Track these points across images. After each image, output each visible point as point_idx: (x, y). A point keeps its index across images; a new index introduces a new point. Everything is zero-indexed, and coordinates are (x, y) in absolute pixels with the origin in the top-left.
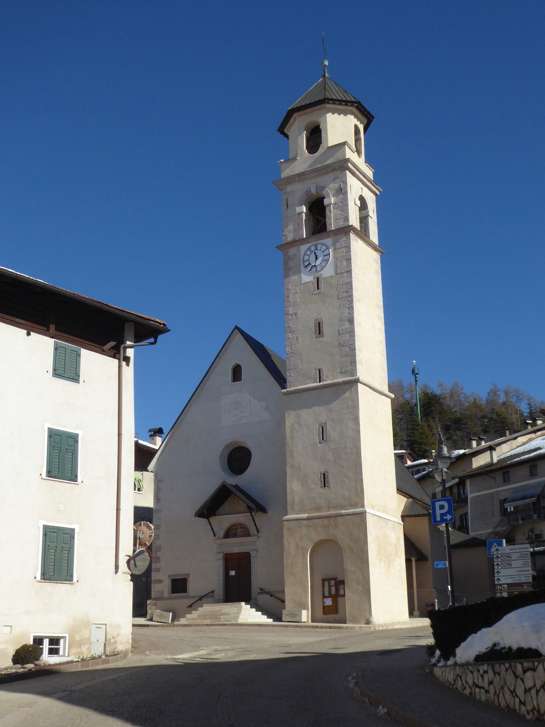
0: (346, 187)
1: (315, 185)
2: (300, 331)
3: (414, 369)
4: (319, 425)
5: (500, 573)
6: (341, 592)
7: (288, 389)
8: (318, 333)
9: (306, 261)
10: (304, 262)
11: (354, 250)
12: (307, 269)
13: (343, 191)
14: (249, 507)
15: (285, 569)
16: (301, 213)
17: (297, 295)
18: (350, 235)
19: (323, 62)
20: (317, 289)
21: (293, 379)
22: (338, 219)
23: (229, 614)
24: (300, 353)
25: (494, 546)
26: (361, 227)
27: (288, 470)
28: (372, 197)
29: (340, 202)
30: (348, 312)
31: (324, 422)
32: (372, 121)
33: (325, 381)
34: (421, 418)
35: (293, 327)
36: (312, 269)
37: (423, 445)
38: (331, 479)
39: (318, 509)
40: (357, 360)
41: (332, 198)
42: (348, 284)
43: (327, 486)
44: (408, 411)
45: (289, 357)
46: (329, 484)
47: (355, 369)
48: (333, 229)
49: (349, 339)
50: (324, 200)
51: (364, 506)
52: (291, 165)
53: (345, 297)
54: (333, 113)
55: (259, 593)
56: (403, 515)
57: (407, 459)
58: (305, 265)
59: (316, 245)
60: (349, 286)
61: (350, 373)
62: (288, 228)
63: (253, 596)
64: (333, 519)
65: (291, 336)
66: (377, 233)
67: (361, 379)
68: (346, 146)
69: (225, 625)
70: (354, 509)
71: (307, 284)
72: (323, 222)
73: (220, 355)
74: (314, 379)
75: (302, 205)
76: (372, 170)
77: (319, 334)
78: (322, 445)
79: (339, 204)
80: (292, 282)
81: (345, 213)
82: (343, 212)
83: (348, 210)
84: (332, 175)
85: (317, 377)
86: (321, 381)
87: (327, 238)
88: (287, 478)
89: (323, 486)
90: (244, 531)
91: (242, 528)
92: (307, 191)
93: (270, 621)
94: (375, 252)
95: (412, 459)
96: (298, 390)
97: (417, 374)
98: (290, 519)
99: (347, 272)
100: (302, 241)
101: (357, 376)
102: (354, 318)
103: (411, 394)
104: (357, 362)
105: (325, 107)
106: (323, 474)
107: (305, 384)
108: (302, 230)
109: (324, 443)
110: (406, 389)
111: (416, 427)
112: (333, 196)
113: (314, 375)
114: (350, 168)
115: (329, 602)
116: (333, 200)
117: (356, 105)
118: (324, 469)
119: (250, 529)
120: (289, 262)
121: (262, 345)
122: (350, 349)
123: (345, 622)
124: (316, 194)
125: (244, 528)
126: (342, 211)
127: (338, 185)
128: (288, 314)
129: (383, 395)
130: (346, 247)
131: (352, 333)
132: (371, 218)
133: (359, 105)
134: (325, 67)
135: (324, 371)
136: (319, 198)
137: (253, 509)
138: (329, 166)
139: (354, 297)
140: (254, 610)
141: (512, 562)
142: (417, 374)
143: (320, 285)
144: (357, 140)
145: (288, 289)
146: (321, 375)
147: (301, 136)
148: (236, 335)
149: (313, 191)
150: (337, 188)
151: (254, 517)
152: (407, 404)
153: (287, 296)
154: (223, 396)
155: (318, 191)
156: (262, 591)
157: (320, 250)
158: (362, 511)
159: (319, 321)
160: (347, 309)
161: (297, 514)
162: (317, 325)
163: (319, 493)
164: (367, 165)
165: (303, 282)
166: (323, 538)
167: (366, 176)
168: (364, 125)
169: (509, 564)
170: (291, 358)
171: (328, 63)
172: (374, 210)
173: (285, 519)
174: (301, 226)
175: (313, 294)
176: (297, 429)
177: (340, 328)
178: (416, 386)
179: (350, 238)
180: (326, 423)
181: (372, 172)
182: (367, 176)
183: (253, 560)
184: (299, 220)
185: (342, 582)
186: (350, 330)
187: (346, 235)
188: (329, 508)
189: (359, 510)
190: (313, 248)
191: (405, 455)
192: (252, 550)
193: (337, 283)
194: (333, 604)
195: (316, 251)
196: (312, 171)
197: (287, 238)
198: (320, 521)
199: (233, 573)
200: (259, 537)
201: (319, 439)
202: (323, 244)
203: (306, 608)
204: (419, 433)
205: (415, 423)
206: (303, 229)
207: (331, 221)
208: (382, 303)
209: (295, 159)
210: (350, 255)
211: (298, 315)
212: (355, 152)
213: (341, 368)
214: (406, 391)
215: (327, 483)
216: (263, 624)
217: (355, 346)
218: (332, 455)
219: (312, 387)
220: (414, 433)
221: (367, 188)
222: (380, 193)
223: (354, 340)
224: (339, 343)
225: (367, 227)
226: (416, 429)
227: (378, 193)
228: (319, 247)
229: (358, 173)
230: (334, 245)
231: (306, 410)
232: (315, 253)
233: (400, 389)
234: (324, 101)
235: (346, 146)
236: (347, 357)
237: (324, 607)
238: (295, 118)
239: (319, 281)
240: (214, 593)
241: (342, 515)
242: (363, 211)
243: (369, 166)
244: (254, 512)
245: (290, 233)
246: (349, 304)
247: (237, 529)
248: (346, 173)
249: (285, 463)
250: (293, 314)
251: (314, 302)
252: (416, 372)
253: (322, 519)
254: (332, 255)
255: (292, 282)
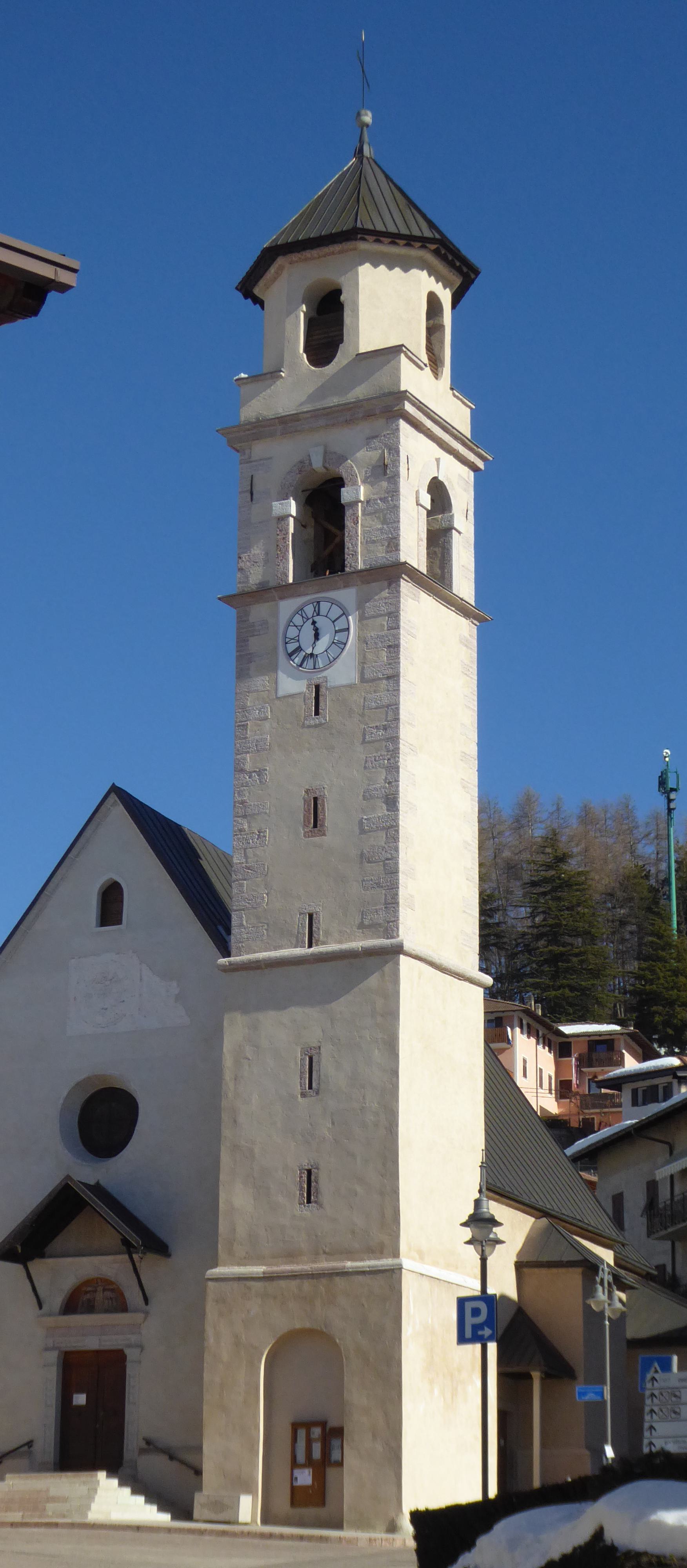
0: (396, 462)
1: (321, 450)
2: (269, 816)
3: (666, 774)
4: (303, 1053)
5: (655, 1429)
6: (335, 1455)
7: (232, 959)
8: (312, 825)
9: (292, 641)
10: (286, 643)
11: (409, 621)
12: (293, 661)
13: (388, 472)
14: (126, 1243)
15: (207, 1397)
16: (283, 518)
17: (267, 725)
18: (399, 586)
19: (359, 115)
20: (315, 715)
21: (248, 933)
22: (374, 542)
23: (65, 1500)
24: (266, 869)
25: (653, 1370)
26: (430, 567)
27: (225, 1158)
28: (465, 476)
29: (381, 499)
30: (386, 778)
31: (315, 1044)
32: (472, 281)
33: (324, 943)
34: (678, 924)
35: (253, 803)
36: (306, 662)
37: (679, 1006)
38: (325, 1184)
39: (291, 1256)
40: (400, 897)
41: (362, 488)
42: (388, 708)
43: (316, 1202)
44: (642, 899)
45: (240, 880)
46: (320, 1196)
47: (394, 921)
48: (360, 566)
49: (384, 845)
50: (343, 489)
51: (399, 1254)
52: (265, 390)
53: (381, 740)
54: (375, 265)
55: (142, 1451)
56: (520, 1260)
57: (624, 1051)
58: (290, 651)
59: (318, 603)
60: (392, 710)
61: (382, 929)
62: (250, 552)
63: (127, 1455)
64: (324, 1281)
65: (246, 827)
66: (473, 569)
67: (407, 946)
68: (402, 355)
69: (56, 1525)
70: (376, 1259)
71: (290, 700)
72: (337, 540)
73: (70, 855)
74: (297, 937)
75: (287, 498)
76: (470, 404)
77: (315, 826)
78: (306, 1100)
79: (377, 504)
80: (255, 691)
81: (392, 530)
82: (385, 526)
83: (399, 522)
84: (364, 428)
85: (304, 934)
86: (314, 944)
87: (345, 587)
88: (222, 1177)
89: (306, 1201)
90: (111, 1298)
91: (109, 1290)
92: (301, 462)
93: (165, 1518)
94: (463, 619)
95: (640, 1051)
96: (258, 962)
97: (672, 790)
98: (222, 1276)
99: (388, 678)
100: (284, 591)
101: (399, 939)
102: (398, 794)
103: (658, 844)
104: (400, 904)
105: (355, 249)
106: (306, 1172)
107: (276, 949)
108: (284, 560)
109: (311, 1096)
110: (642, 830)
111: (661, 953)
112: (364, 482)
113: (297, 927)
114: (410, 414)
115: (305, 1477)
116: (363, 492)
117: (433, 247)
118: (309, 1161)
119: (127, 1295)
120: (251, 639)
121: (179, 828)
122: (385, 869)
123: (339, 1526)
124: (324, 470)
125: (112, 1290)
126: (384, 522)
127: (378, 455)
128: (242, 771)
129: (464, 980)
130: (389, 614)
131: (392, 830)
132: (460, 533)
133: (441, 247)
134: (365, 128)
135: (321, 921)
136: (330, 478)
137: (134, 1247)
138: (357, 404)
139: (401, 741)
140: (127, 1491)
141: (682, 1407)
142: (672, 790)
143: (321, 704)
144: (433, 330)
145: (244, 708)
146: (314, 929)
147: (293, 316)
148: (112, 808)
149: (317, 464)
150: (373, 462)
151: (137, 1264)
152: (642, 877)
153: (243, 725)
154: (73, 960)
155: (328, 465)
156: (150, 1446)
157: (326, 616)
158: (393, 1266)
159: (316, 796)
160: (384, 771)
161: (239, 1264)
162: (309, 805)
163: (295, 1216)
164: (457, 394)
165: (281, 693)
166: (298, 1326)
167: (449, 429)
168: (453, 291)
169: (675, 1412)
170: (245, 880)
171: (373, 118)
172: (467, 511)
173: (210, 1277)
174: (283, 550)
175: (303, 726)
176: (251, 1058)
177: (365, 817)
178: (669, 825)
179: (399, 592)
180: (320, 1047)
181: (469, 410)
182: (454, 428)
183: (130, 1370)
184: (278, 535)
185: (339, 1432)
186: (388, 824)
187: (390, 585)
188: (316, 1254)
189: (386, 1262)
190: (309, 610)
191: (619, 1039)
192: (130, 1346)
193: (364, 703)
194: (316, 1484)
195: (316, 619)
196: (316, 414)
197: (247, 577)
198: (293, 1284)
199: (80, 1399)
200: (147, 1313)
201: (301, 1086)
202: (333, 602)
203: (249, 1489)
204: (669, 971)
205: (658, 941)
206: (287, 560)
207: (356, 545)
208: (477, 748)
209: (274, 374)
210: (397, 637)
211: (266, 774)
212: (423, 365)
213: (362, 915)
214: (642, 835)
215: (315, 1194)
216: (146, 1524)
217: (397, 864)
218: (330, 1126)
219: (291, 958)
220: (654, 970)
221: (452, 457)
222: (485, 465)
223: (397, 850)
224: (359, 853)
225: (446, 555)
226: (659, 959)
227: (481, 464)
228: (324, 607)
229: (428, 423)
230: (360, 605)
231: (272, 1014)
232: (314, 623)
233: (625, 827)
234: (353, 234)
235: (402, 355)
236: (378, 889)
237: (294, 1490)
238: (281, 268)
239: (320, 693)
240: (31, 1446)
241: (344, 1274)
242: (440, 516)
243: (461, 397)
244: (137, 1253)
245: (255, 564)
246: (389, 759)
247: (95, 1291)
248: (398, 425)
249: (216, 1137)
250: (255, 771)
251: (307, 745)
252: (671, 784)
253: (298, 1281)
254: (355, 629)
255: (255, 691)
